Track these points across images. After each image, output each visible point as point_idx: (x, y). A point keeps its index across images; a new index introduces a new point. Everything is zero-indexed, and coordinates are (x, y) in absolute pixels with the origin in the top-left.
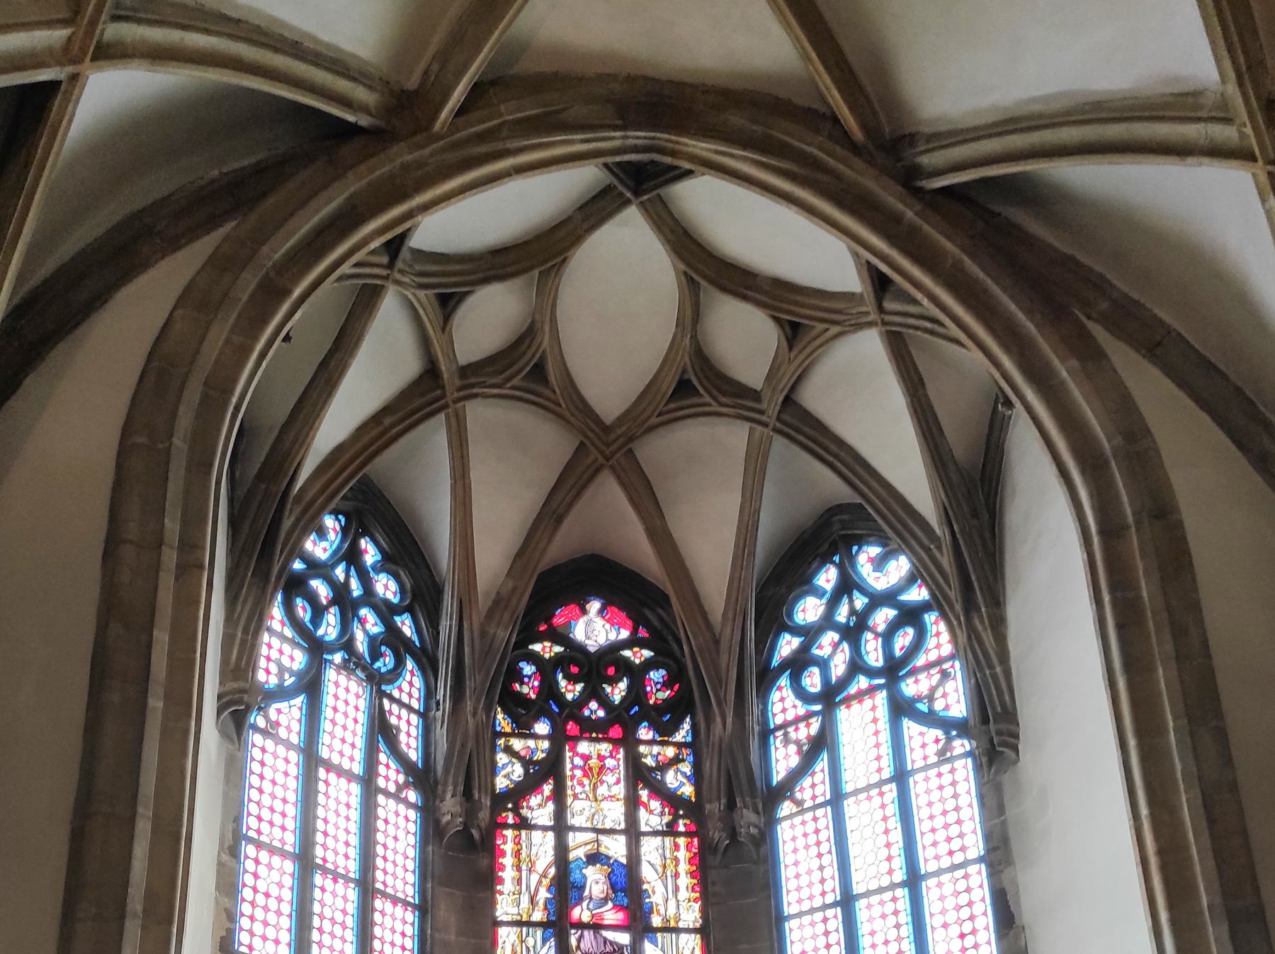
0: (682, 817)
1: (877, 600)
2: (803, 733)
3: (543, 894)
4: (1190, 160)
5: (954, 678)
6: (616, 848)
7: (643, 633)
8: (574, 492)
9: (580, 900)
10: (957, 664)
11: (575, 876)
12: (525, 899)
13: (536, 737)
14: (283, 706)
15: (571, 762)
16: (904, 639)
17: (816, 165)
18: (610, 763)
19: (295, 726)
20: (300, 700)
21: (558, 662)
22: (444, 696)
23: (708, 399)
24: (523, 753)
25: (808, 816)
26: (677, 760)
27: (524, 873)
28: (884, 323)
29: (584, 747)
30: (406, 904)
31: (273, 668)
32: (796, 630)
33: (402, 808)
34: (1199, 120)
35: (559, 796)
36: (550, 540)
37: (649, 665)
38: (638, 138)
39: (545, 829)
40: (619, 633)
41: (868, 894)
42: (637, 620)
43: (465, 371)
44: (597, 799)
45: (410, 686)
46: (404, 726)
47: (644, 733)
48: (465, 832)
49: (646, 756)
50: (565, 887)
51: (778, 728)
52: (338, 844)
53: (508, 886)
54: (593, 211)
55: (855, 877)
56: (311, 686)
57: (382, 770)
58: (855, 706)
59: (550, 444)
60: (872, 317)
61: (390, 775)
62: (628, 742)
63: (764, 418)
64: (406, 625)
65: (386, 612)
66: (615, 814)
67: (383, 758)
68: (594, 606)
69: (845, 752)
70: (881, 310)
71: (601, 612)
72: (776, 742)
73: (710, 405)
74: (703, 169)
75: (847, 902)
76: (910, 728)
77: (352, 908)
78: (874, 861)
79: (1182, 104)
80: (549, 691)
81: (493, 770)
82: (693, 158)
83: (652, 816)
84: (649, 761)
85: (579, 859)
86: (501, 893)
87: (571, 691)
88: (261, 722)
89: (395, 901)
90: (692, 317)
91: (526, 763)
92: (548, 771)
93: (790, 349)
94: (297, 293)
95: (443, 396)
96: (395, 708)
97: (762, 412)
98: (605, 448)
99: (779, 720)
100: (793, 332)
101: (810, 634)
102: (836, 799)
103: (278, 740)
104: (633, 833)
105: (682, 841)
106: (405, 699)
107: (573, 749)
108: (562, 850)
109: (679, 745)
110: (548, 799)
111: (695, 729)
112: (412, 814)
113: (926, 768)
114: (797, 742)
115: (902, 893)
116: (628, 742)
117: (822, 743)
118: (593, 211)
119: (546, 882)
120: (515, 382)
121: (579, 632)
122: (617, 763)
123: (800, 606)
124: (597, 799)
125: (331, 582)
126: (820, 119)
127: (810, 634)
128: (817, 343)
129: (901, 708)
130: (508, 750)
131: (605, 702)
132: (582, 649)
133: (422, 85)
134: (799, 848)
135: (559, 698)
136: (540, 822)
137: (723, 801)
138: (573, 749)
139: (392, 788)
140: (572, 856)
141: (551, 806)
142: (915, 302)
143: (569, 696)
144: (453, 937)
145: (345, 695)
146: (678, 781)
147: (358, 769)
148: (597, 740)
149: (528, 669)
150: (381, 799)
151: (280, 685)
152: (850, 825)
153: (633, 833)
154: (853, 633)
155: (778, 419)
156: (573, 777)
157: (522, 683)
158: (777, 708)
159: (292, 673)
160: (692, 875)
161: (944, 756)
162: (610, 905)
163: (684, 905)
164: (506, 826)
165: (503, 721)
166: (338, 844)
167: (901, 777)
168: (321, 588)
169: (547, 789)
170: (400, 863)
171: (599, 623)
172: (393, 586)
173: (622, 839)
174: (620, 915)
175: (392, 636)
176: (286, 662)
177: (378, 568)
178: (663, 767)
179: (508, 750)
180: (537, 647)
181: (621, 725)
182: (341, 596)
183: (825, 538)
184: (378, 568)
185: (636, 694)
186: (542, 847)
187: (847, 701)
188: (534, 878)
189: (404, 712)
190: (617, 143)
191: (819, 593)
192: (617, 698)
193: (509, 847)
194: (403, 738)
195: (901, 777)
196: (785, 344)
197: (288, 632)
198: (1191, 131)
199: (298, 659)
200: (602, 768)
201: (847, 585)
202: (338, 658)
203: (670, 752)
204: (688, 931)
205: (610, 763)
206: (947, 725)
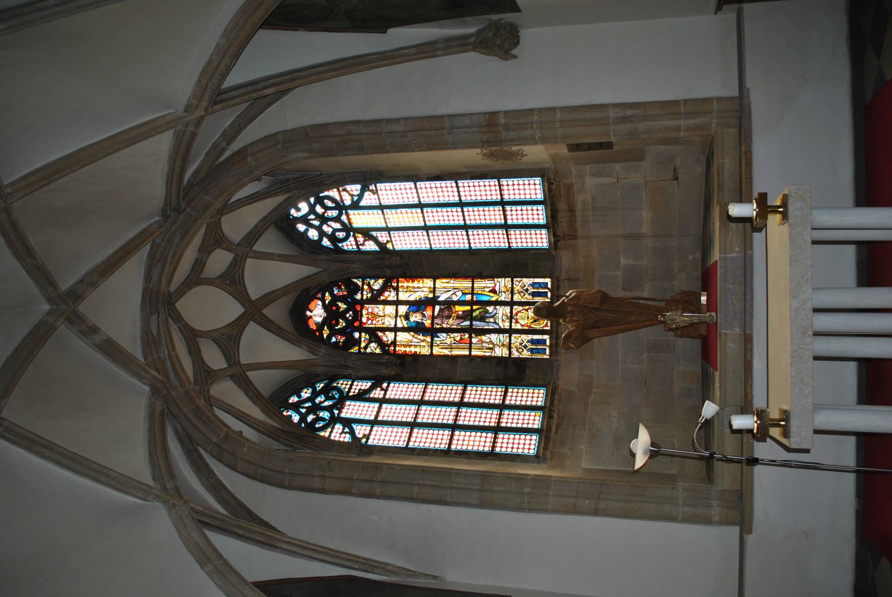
2: (361, 239)
3: (421, 337)
6: (403, 309)
7: (319, 296)
9: (423, 324)
11: (413, 325)
12: (422, 344)
13: (360, 337)
14: (357, 432)
15: (369, 325)
16: (329, 203)
18: (370, 310)
19: (364, 427)
20: (354, 426)
21: (331, 328)
25: (393, 239)
26: (369, 285)
29: (364, 320)
30: (425, 388)
31: (343, 435)
32: (320, 239)
33: (390, 389)
35: (384, 330)
37: (332, 294)
39: (396, 336)
41: (424, 221)
42: (314, 298)
44: (384, 315)
45: (343, 384)
46: (358, 388)
47: (358, 297)
50: (418, 329)
52: (406, 413)
53: (418, 350)
54: (179, 319)
55: (417, 225)
56: (348, 423)
57: (376, 396)
58: (352, 221)
59: (252, 329)
61: (377, 393)
62: (362, 303)
64: (320, 386)
65: (315, 394)
66: (390, 309)
67: (372, 396)
69: (369, 225)
71: (311, 311)
72: (363, 248)
75: (426, 228)
76: (362, 204)
77: (429, 408)
78: (414, 218)
80: (342, 332)
81: (373, 354)
83: (391, 295)
84: (369, 295)
87: (342, 324)
88: (364, 441)
89: (424, 392)
90: (210, 282)
91: (370, 341)
92: (373, 334)
96: (352, 390)
98: (254, 311)
99: (355, 247)
101: (322, 234)
102: (388, 229)
103: (370, 434)
104: (397, 303)
105: (400, 285)
106: (348, 386)
107: (365, 324)
108: (403, 330)
109: (363, 284)
111: (357, 278)
112: (392, 385)
113: (379, 199)
114: (364, 241)
115: (425, 210)
116: (362, 303)
117: (367, 233)
121: (319, 320)
122: (370, 308)
123: (311, 237)
124: (384, 315)
125: (307, 414)
127: (322, 234)
129: (355, 206)
130: (366, 348)
131: (346, 311)
132: (325, 320)
133: (148, 385)
134: (402, 242)
138: (365, 324)
139: (383, 392)
140: (406, 326)
141: (387, 333)
145: (352, 410)
146: (377, 285)
147: (377, 405)
148: (362, 315)
149: (334, 339)
150: (387, 396)
151: (349, 433)
152: (398, 225)
153: (397, 303)
154: (324, 220)
158: (350, 247)
159: (344, 429)
160: (413, 281)
161: (375, 192)
163: (425, 285)
164: (395, 349)
165: (355, 350)
166: (406, 413)
167: (381, 207)
168: (310, 418)
169: (380, 334)
170: (412, 390)
171: (315, 312)
172: (305, 390)
173: (400, 307)
175: (325, 391)
176: (340, 431)
177: (299, 396)
178: (371, 289)
179: (366, 348)
180: (325, 336)
181: (356, 306)
182: (310, 411)
183: (285, 225)
184: (299, 396)
185: (343, 299)
186: (402, 337)
187: (350, 223)
189: (354, 387)
191: (307, 230)
192: (345, 306)
193: (403, 349)
194: (363, 388)
195: (381, 207)
197: (329, 430)
199: (339, 427)
201: (304, 220)
202: (336, 412)
203: (366, 287)
204: (434, 284)
205: (370, 310)
206: (363, 191)
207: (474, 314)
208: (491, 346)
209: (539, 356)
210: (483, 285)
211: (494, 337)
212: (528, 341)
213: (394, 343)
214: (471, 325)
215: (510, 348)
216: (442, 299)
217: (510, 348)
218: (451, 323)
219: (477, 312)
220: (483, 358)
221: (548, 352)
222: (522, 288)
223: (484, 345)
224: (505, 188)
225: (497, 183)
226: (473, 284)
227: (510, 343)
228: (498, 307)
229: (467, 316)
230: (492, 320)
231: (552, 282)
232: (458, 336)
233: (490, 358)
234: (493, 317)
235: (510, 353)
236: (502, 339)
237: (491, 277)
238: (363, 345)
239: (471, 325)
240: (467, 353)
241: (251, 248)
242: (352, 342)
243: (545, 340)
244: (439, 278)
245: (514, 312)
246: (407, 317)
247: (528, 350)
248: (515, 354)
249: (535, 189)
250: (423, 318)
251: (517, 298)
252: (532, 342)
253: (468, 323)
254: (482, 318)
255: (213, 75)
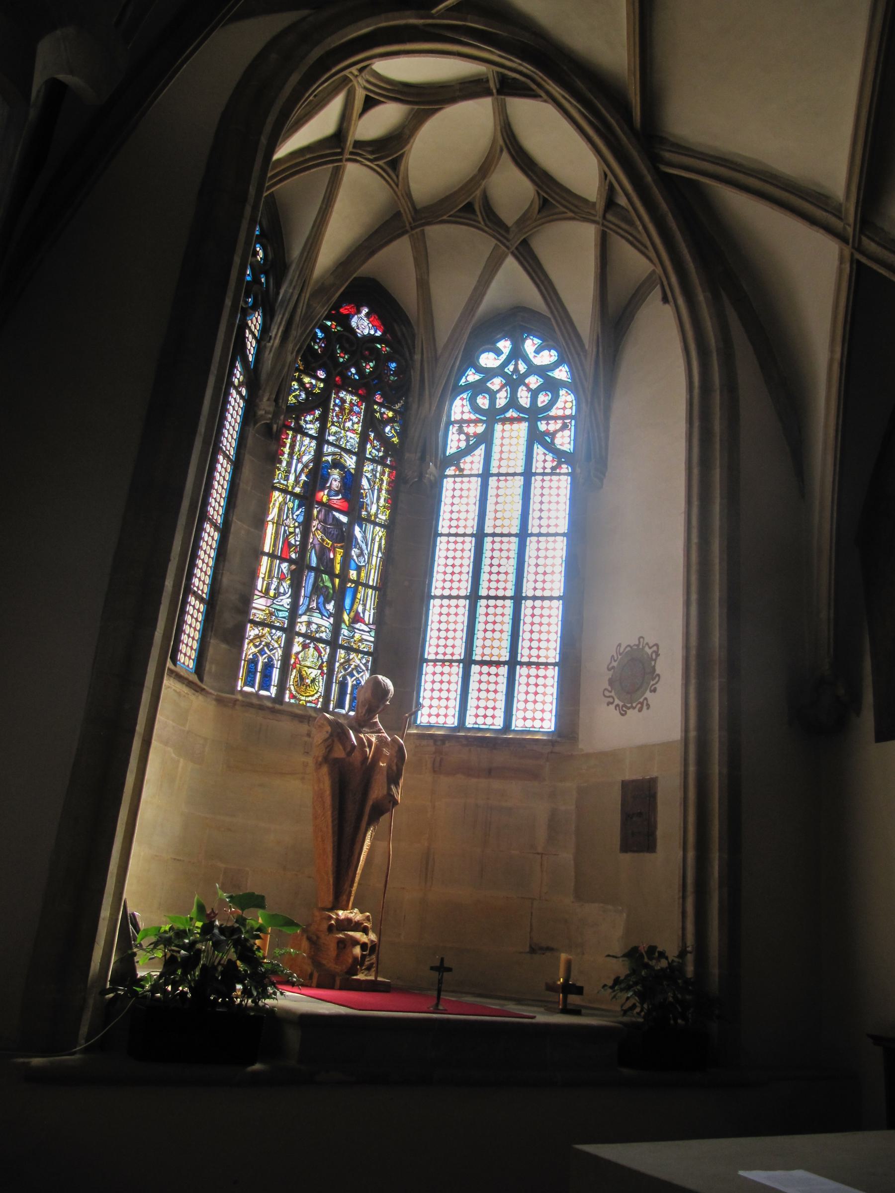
0: (390, 456)
1: (533, 369)
4: (815, 228)
5: (570, 430)
6: (350, 462)
8: (554, 298)
9: (323, 489)
10: (573, 422)
12: (292, 478)
17: (608, 127)
18: (356, 409)
21: (339, 337)
22: (276, 335)
23: (480, 219)
24: (308, 386)
27: (295, 462)
28: (603, 225)
32: (479, 369)
34: (826, 211)
35: (323, 420)
36: (364, 262)
38: (526, 68)
40: (376, 332)
43: (358, 144)
47: (378, 398)
48: (269, 427)
49: (377, 412)
50: (317, 475)
51: (456, 422)
54: (468, 89)
60: (597, 218)
63: (508, 243)
66: (352, 440)
68: (365, 310)
70: (604, 217)
72: (453, 429)
73: (479, 223)
74: (550, 101)
76: (539, 450)
79: (821, 199)
80: (329, 351)
81: (290, 391)
82: (548, 93)
85: (327, 461)
86: (279, 469)
90: (485, 168)
91: (309, 393)
92: (319, 402)
93: (539, 212)
94: (334, 70)
95: (341, 154)
97: (508, 240)
100: (545, 204)
105: (387, 470)
107: (337, 393)
108: (319, 453)
110: (317, 420)
113: (544, 474)
114: (467, 435)
116: (367, 399)
118: (468, 89)
119: (306, 470)
120: (381, 163)
126: (621, 106)
127: (489, 373)
128: (555, 217)
129: (535, 437)
131: (360, 371)
132: (352, 331)
135: (334, 359)
136: (311, 432)
137: (419, 455)
141: (317, 424)
142: (636, 228)
143: (341, 360)
144: (249, 489)
155: (517, 248)
156: (334, 410)
157: (315, 342)
162: (340, 497)
164: (290, 428)
174: (345, 504)
181: (365, 389)
186: (307, 448)
188: (300, 466)
190: (514, 65)
196: (536, 207)
198: (819, 213)
200: (351, 410)
201: (517, 353)
205: (356, 409)
206: (559, 454)
207: (325, 577)
208: (272, 593)
209: (242, 673)
210: (367, 605)
211: (286, 601)
212: (270, 658)
213: (299, 430)
214: (311, 569)
215: (262, 624)
216: (357, 529)
217: (262, 624)
218: (317, 536)
219: (329, 584)
220: (253, 575)
221: (247, 689)
222: (268, 645)
223: (275, 582)
224: (446, 669)
225: (456, 657)
226: (371, 587)
227: (271, 626)
228: (331, 620)
229: (325, 566)
230: (314, 605)
231: (269, 698)
232: (295, 540)
233: (252, 585)
234: (318, 608)
235: (256, 624)
236: (281, 614)
237: (379, 620)
238: (307, 380)
239: (311, 569)
240: (267, 548)
241: (513, 254)
242: (310, 364)
243: (268, 690)
244: (389, 537)
245: (321, 646)
246: (337, 464)
247: (255, 655)
248: (252, 632)
249: (438, 715)
250: (331, 492)
251: (341, 653)
252: (269, 666)
253: (314, 563)
254: (317, 589)
255: (422, 361)
